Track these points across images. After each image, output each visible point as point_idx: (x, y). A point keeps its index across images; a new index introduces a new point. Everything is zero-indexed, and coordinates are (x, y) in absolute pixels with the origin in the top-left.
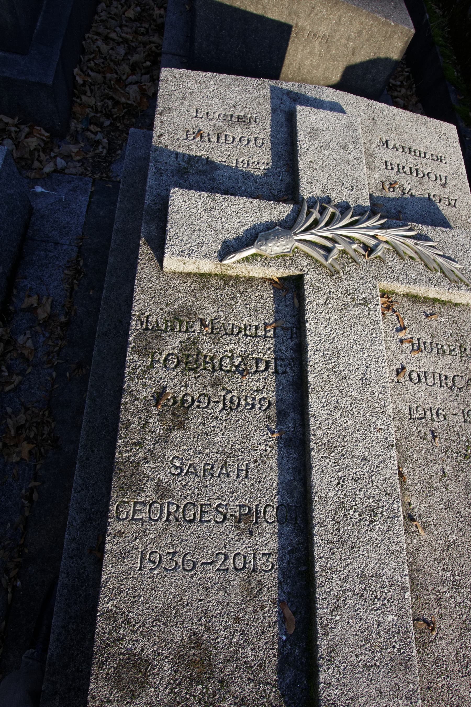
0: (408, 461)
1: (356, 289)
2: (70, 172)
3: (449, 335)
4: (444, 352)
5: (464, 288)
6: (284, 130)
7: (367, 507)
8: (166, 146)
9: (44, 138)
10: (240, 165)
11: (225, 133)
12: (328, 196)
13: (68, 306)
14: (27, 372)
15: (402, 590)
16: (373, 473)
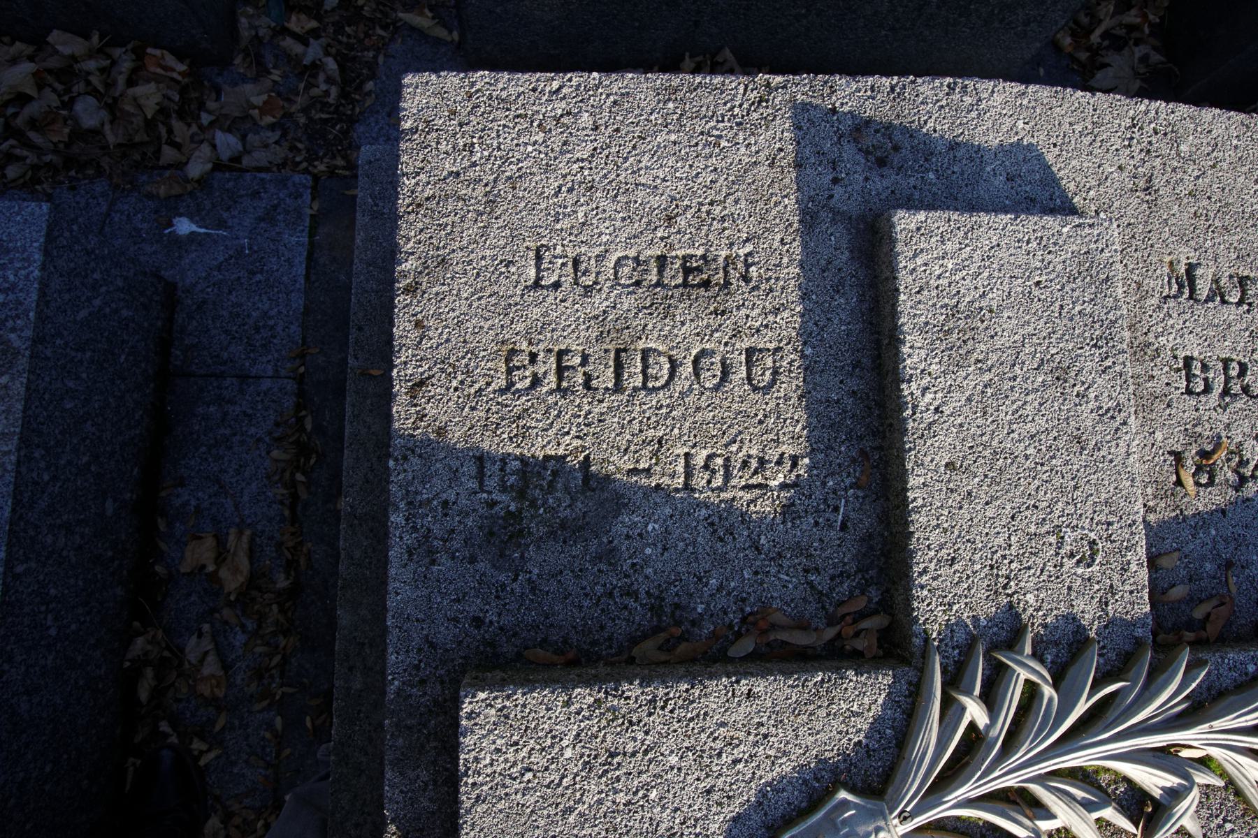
2: (254, 164)
6: (846, 302)
8: (441, 431)
9: (175, 75)
10: (700, 480)
11: (641, 345)
12: (1010, 606)
13: (290, 544)
14: (218, 728)
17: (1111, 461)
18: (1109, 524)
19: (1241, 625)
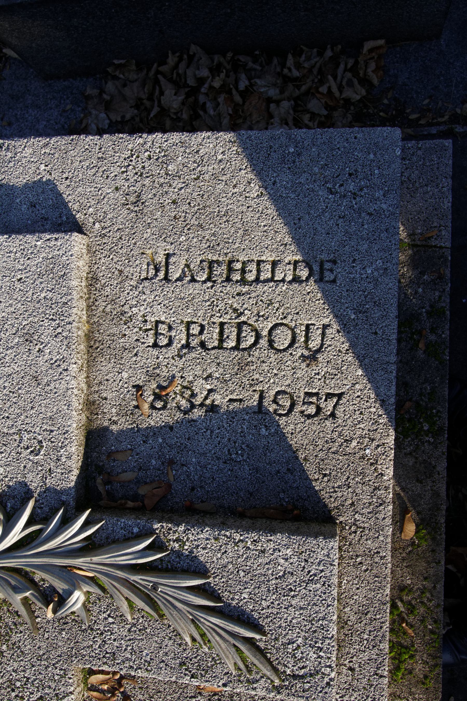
17: (56, 393)
18: (52, 431)
19: (176, 502)
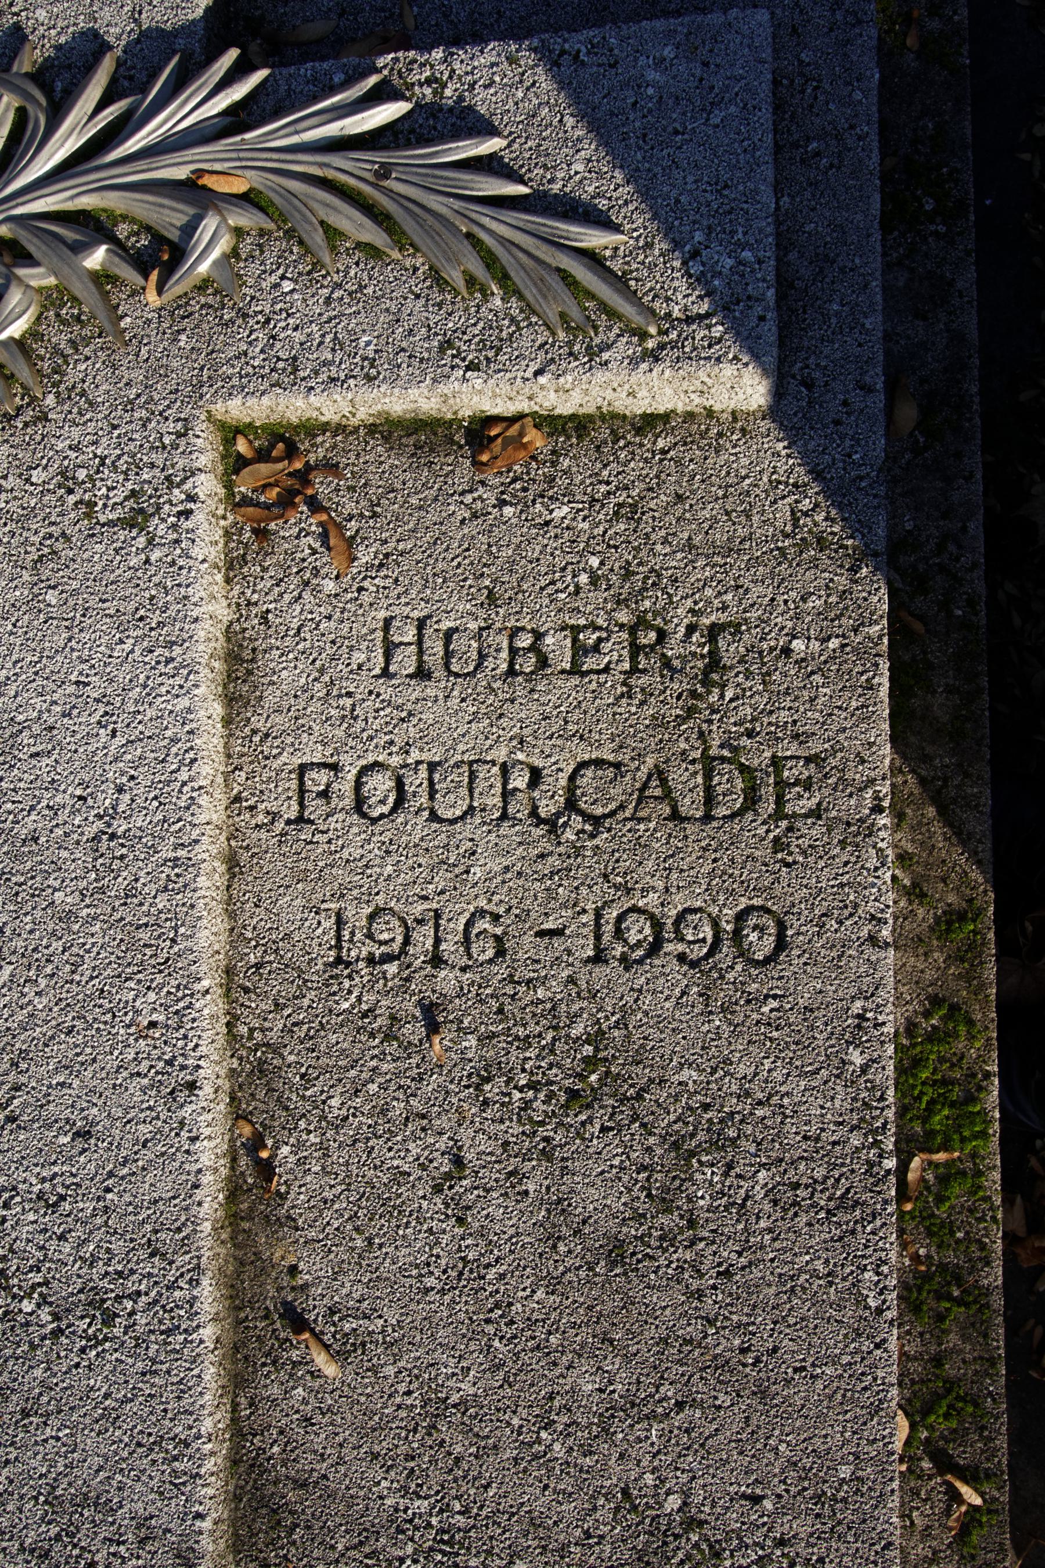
0: (302, 1124)
1: (103, 459)
3: (584, 579)
4: (543, 662)
5: (625, 347)
7: (81, 1291)
15: (178, 1556)
16: (110, 1182)
